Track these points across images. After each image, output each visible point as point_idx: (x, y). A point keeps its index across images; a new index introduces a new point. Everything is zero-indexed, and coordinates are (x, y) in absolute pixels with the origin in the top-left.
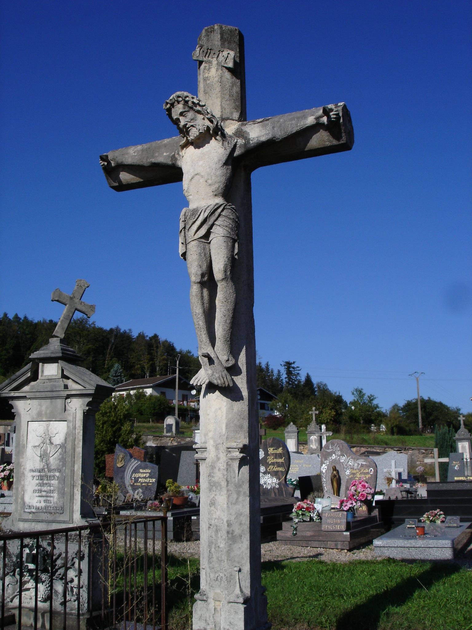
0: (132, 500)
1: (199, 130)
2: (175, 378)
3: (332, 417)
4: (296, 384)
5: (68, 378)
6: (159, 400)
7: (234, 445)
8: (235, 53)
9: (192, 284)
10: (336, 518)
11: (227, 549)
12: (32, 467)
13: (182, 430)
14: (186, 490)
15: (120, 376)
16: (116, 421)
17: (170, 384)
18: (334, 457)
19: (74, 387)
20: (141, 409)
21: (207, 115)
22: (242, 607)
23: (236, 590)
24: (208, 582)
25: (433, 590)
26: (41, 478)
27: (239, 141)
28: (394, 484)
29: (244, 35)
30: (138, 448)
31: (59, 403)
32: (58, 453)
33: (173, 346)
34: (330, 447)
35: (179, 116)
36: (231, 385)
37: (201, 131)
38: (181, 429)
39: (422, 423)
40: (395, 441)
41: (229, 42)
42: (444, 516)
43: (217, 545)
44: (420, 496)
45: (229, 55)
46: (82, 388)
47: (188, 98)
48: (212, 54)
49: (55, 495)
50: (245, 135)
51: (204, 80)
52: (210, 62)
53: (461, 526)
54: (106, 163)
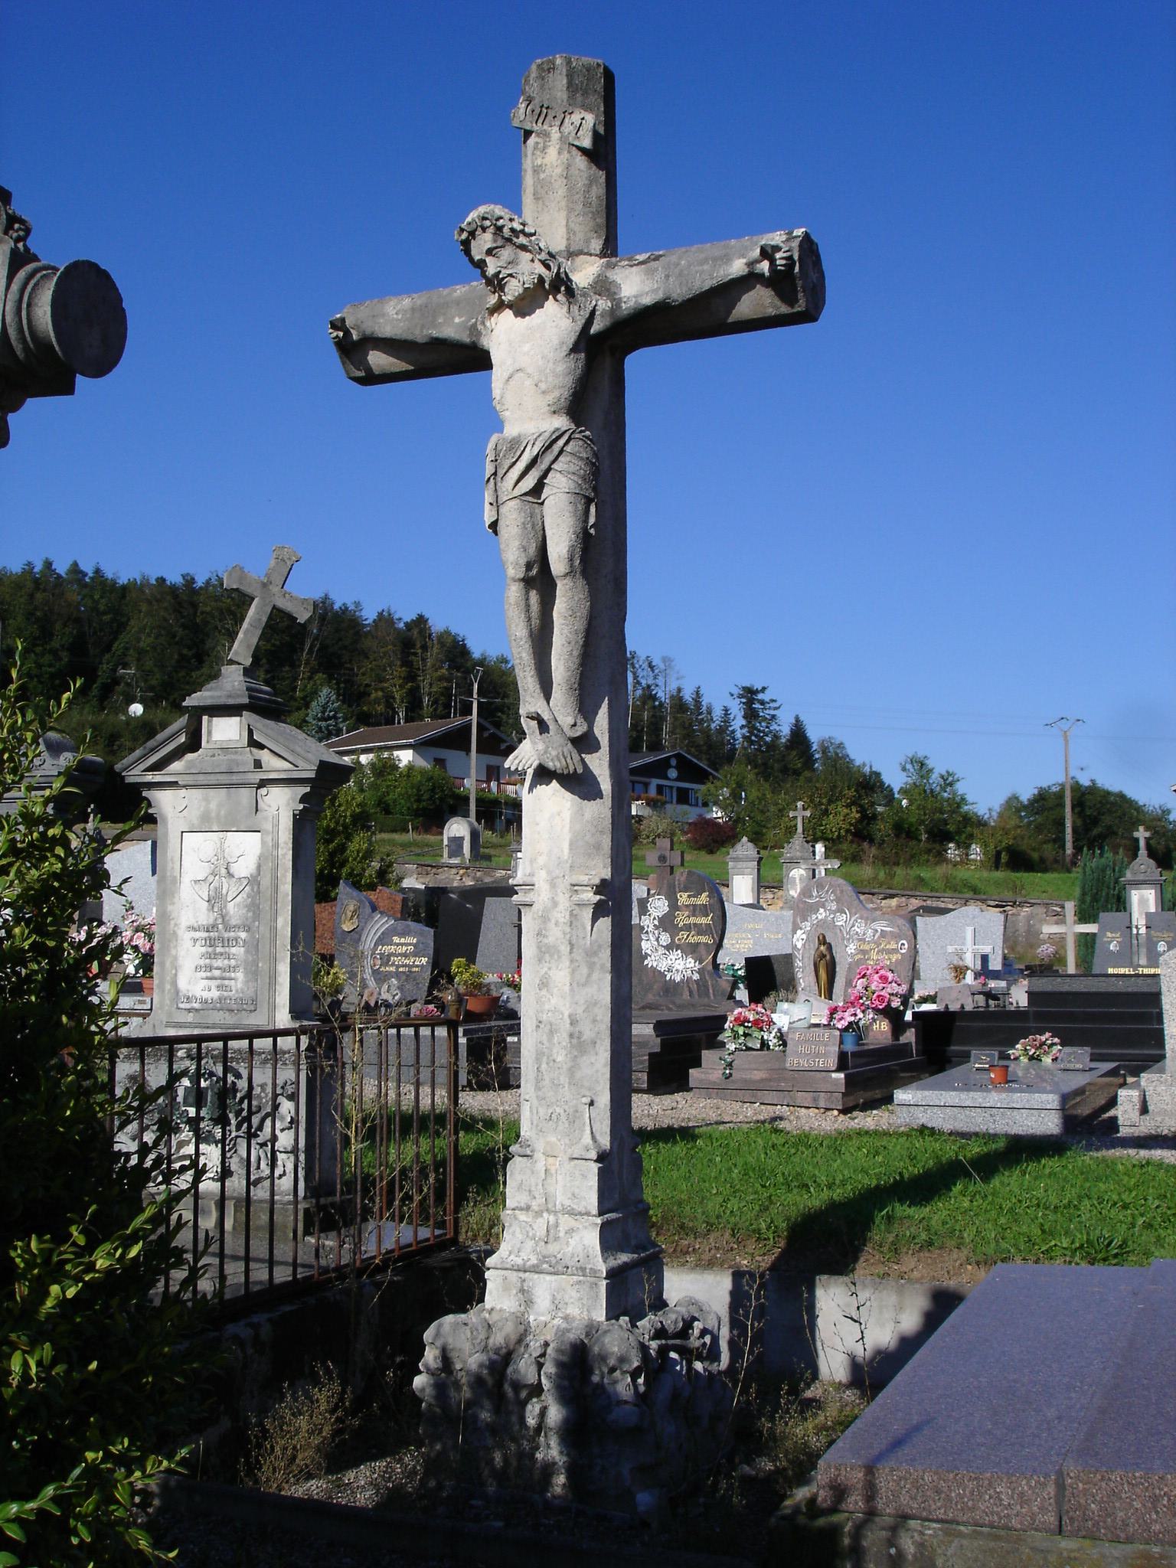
0: (377, 1002)
1: (524, 283)
2: (469, 726)
3: (851, 825)
4: (766, 743)
5: (261, 747)
6: (430, 779)
7: (584, 879)
8: (597, 116)
9: (509, 581)
10: (817, 1043)
11: (570, 1064)
12: (192, 922)
13: (487, 851)
14: (496, 983)
15: (335, 717)
16: (333, 830)
17: (457, 740)
18: (822, 914)
19: (274, 765)
20: (387, 798)
21: (539, 254)
22: (594, 1167)
23: (585, 1137)
24: (535, 1123)
25: (996, 1182)
26: (211, 942)
27: (599, 303)
28: (969, 978)
29: (615, 73)
30: (388, 890)
31: (245, 795)
32: (244, 895)
33: (464, 645)
34: (815, 893)
35: (484, 255)
36: (580, 771)
37: (526, 286)
38: (483, 847)
39: (1073, 842)
40: (997, 884)
41: (585, 93)
42: (1059, 1047)
43: (551, 1058)
44: (1015, 1005)
45: (584, 122)
46: (291, 766)
47: (501, 221)
48: (550, 117)
49: (240, 975)
50: (613, 289)
51: (535, 171)
52: (546, 135)
53: (1091, 1069)
54: (341, 334)
